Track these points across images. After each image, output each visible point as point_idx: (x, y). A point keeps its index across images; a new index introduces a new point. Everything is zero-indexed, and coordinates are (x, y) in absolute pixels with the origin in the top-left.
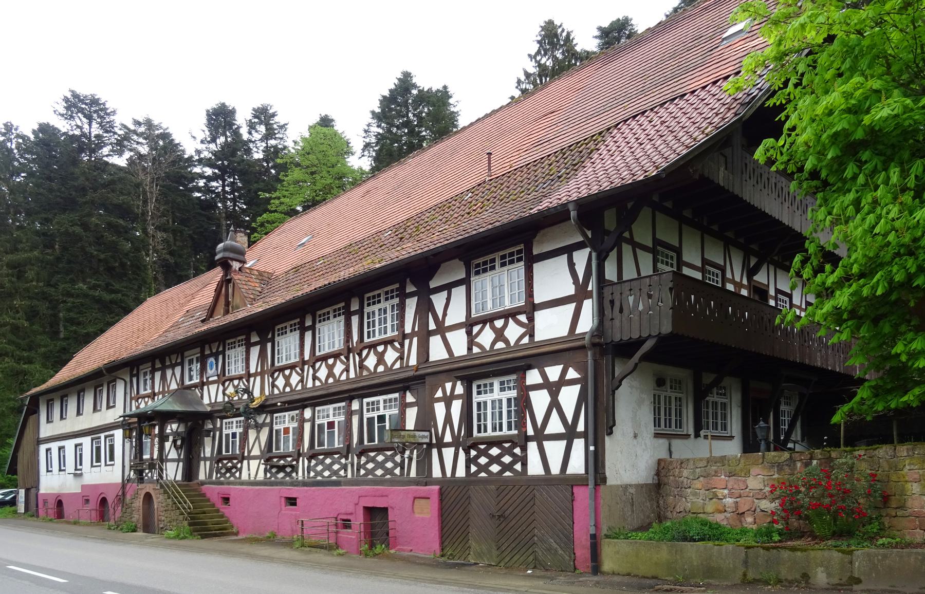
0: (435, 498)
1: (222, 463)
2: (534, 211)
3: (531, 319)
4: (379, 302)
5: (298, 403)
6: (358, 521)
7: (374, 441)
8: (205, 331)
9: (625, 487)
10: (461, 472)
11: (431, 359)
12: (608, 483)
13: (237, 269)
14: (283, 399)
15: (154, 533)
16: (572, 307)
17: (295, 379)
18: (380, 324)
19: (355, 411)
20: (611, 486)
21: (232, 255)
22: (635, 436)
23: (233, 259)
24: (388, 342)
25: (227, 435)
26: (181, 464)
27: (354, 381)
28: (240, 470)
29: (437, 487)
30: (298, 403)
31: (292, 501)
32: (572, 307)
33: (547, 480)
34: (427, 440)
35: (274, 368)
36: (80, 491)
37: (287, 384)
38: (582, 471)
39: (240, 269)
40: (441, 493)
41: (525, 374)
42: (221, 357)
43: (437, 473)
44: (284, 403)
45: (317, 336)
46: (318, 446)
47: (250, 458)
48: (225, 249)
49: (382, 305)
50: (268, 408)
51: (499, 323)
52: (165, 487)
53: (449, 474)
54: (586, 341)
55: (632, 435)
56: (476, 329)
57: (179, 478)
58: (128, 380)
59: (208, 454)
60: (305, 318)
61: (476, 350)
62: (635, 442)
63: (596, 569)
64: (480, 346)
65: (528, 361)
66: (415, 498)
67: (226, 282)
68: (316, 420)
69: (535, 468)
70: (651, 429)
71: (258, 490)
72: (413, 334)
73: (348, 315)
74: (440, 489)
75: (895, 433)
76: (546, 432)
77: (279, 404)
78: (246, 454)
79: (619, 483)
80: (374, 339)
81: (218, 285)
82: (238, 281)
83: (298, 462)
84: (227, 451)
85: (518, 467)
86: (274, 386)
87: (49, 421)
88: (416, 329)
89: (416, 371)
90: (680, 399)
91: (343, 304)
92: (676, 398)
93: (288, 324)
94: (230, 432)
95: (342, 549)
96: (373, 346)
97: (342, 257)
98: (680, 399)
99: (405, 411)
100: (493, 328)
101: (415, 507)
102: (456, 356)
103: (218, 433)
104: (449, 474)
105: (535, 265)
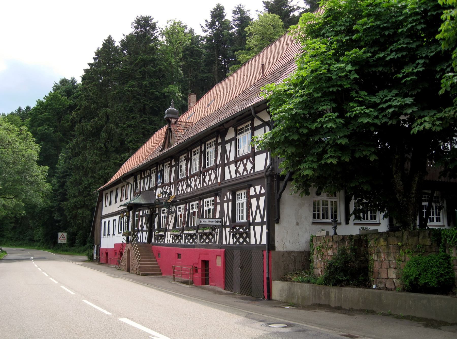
0: (222, 255)
1: (236, 229)
2: (247, 106)
3: (254, 159)
5: (186, 200)
6: (199, 266)
8: (193, 137)
9: (290, 253)
10: (231, 243)
11: (225, 179)
12: (276, 250)
13: (174, 122)
14: (180, 198)
17: (249, 166)
19: (219, 202)
20: (277, 251)
21: (171, 116)
22: (297, 224)
23: (171, 118)
25: (206, 211)
26: (265, 227)
27: (220, 184)
28: (248, 235)
29: (223, 250)
30: (186, 200)
31: (179, 255)
34: (220, 224)
35: (178, 180)
36: (113, 247)
37: (245, 169)
38: (265, 243)
39: (175, 123)
40: (225, 252)
42: (149, 178)
43: (224, 243)
44: (180, 200)
45: (237, 144)
47: (255, 224)
48: (168, 113)
50: (175, 203)
52: (141, 245)
53: (258, 243)
54: (264, 175)
55: (295, 223)
57: (146, 241)
59: (156, 228)
60: (253, 120)
61: (238, 175)
62: (298, 227)
63: (269, 297)
65: (249, 183)
66: (217, 256)
67: (169, 130)
68: (205, 207)
70: (311, 219)
71: (169, 249)
73: (217, 144)
74: (225, 251)
78: (251, 221)
79: (285, 250)
82: (173, 130)
83: (250, 230)
84: (191, 224)
86: (178, 190)
87: (106, 206)
89: (219, 185)
90: (335, 202)
91: (250, 123)
92: (332, 202)
93: (244, 126)
94: (191, 211)
95: (194, 284)
98: (335, 202)
99: (216, 207)
101: (217, 260)
103: (187, 212)
104: (258, 243)
105: (255, 132)
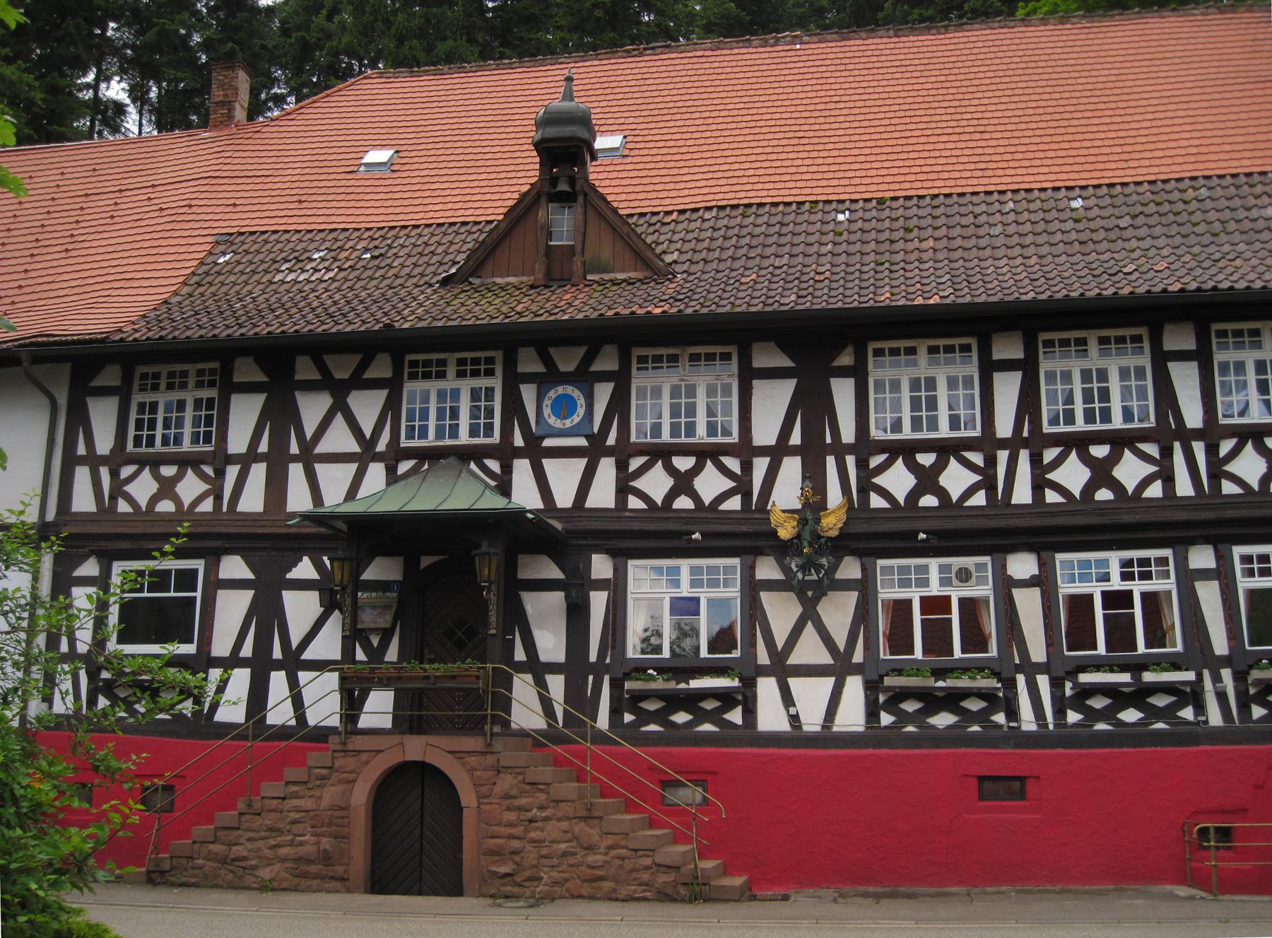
4: (441, 375)
7: (1069, 650)
15: (456, 890)
16: (353, 467)
18: (166, 426)
24: (187, 462)
32: (353, 467)
33: (796, 737)
41: (219, 561)
46: (1148, 645)
49: (448, 384)
51: (168, 471)
56: (635, 463)
58: (63, 401)
64: (130, 499)
69: (771, 717)
72: (251, 456)
75: (590, 687)
76: (304, 657)
77: (922, 536)
80: (151, 450)
81: (520, 201)
85: (736, 716)
88: (1025, 434)
96: (153, 462)
97: (973, 242)
100: (157, 476)
102: (1179, 494)
